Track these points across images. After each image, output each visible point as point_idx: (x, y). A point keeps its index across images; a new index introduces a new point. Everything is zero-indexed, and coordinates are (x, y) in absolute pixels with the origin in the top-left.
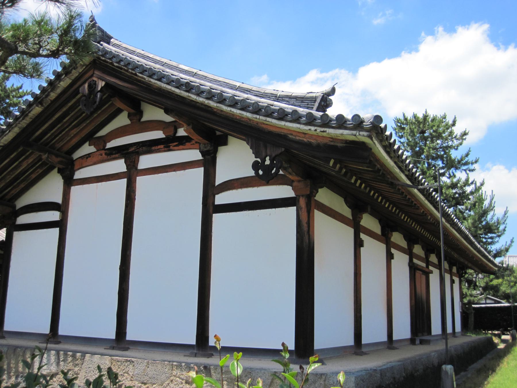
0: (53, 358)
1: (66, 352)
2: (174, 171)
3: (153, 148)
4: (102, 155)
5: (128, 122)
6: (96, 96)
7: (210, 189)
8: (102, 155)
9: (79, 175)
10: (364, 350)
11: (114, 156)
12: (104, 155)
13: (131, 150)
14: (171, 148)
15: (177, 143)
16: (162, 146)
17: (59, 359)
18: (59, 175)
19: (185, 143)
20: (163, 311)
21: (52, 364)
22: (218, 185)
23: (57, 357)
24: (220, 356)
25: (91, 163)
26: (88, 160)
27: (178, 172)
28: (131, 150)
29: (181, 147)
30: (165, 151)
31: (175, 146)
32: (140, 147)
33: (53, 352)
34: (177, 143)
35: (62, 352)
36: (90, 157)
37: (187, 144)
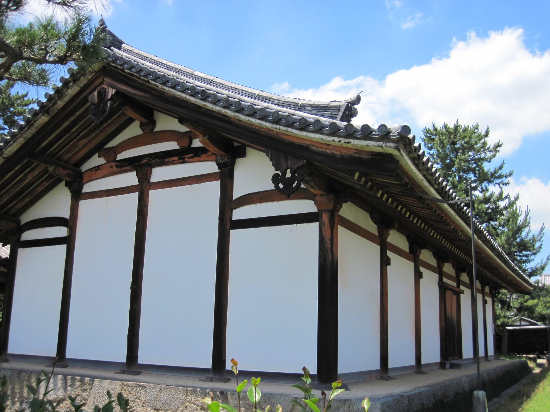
2: (189, 184)
3: (167, 160)
4: (112, 167)
6: (106, 105)
8: (112, 167)
9: (88, 188)
12: (114, 166)
14: (186, 159)
15: (192, 155)
16: (176, 158)
17: (66, 384)
19: (201, 155)
20: (177, 333)
21: (59, 389)
23: (64, 382)
25: (101, 176)
26: (97, 173)
27: (193, 185)
29: (196, 159)
31: (189, 158)
32: (153, 159)
34: (192, 155)
35: (70, 376)
36: (99, 169)
37: (203, 155)
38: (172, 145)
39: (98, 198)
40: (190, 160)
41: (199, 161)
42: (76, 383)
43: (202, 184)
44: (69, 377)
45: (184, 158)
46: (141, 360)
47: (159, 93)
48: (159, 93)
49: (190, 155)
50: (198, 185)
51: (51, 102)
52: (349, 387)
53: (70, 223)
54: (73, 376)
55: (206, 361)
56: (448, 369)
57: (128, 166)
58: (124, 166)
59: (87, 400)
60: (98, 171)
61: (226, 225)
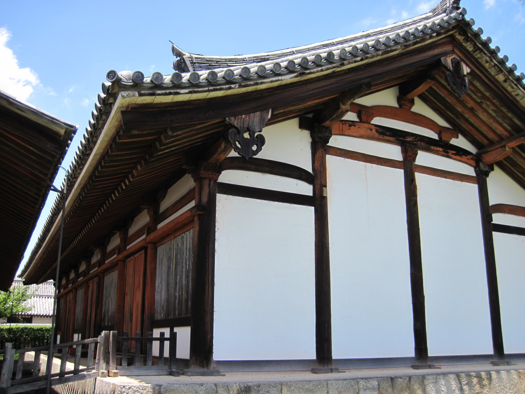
1: (468, 375)
2: (453, 179)
3: (432, 147)
4: (372, 130)
5: (394, 104)
7: (487, 211)
9: (336, 141)
10: (213, 366)
11: (387, 138)
12: (374, 130)
13: (409, 139)
14: (450, 154)
15: (455, 152)
16: (441, 149)
17: (460, 383)
18: (9, 52)
19: (462, 155)
20: (372, 323)
22: (313, 169)
23: (458, 381)
24: (171, 363)
26: (348, 129)
27: (456, 181)
28: (409, 139)
29: (458, 157)
30: (443, 156)
31: (452, 154)
32: (418, 141)
34: (455, 152)
35: (463, 374)
36: (355, 126)
37: (464, 156)
42: (473, 380)
43: (463, 183)
44: (463, 375)
45: (448, 152)
46: (336, 354)
47: (156, 108)
48: (156, 108)
49: (454, 152)
53: (317, 177)
55: (310, 353)
58: (386, 135)
60: (353, 127)
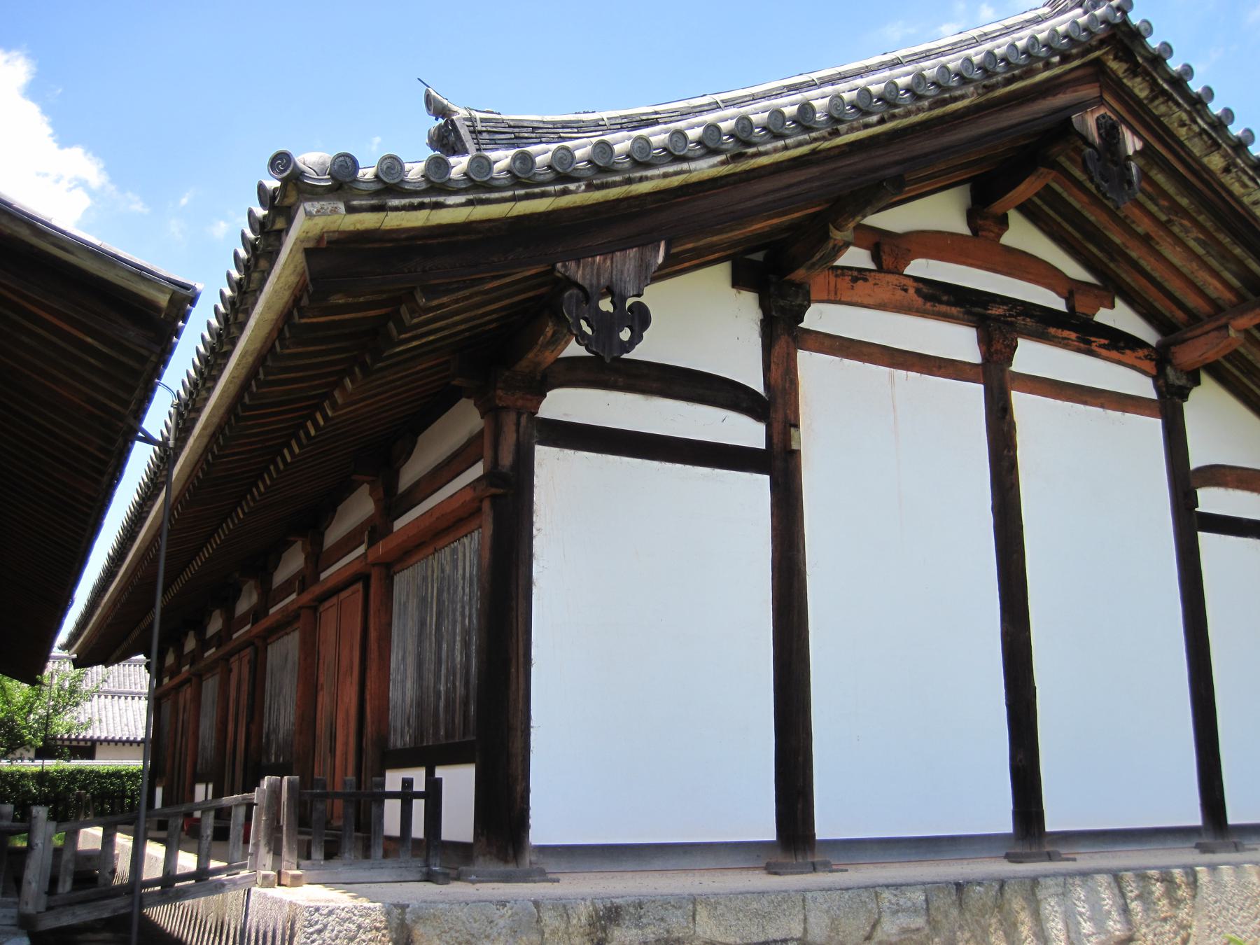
0: (1108, 900)
2: (1102, 406)
3: (1052, 331)
4: (906, 291)
6: (1129, 169)
8: (906, 291)
11: (944, 308)
12: (911, 291)
13: (996, 311)
14: (1094, 347)
15: (1106, 342)
16: (1073, 335)
17: (1123, 896)
19: (1123, 348)
20: (910, 751)
21: (1109, 912)
23: (1116, 891)
25: (871, 301)
27: (1110, 412)
28: (996, 311)
30: (1079, 350)
31: (1100, 346)
32: (1018, 315)
33: (1103, 879)
34: (1106, 342)
35: (1129, 874)
36: (866, 280)
37: (1128, 352)
38: (1057, 303)
39: (864, 361)
40: (1104, 352)
41: (1119, 362)
42: (1154, 889)
43: (1127, 415)
44: (1128, 876)
45: (1089, 343)
49: (1103, 341)
50: (1118, 414)
51: (1211, 125)
52: (818, 867)
54: (1142, 876)
55: (761, 824)
56: (29, 840)
57: (955, 305)
58: (941, 302)
59: (1190, 927)
60: (860, 282)
61: (1190, 524)
